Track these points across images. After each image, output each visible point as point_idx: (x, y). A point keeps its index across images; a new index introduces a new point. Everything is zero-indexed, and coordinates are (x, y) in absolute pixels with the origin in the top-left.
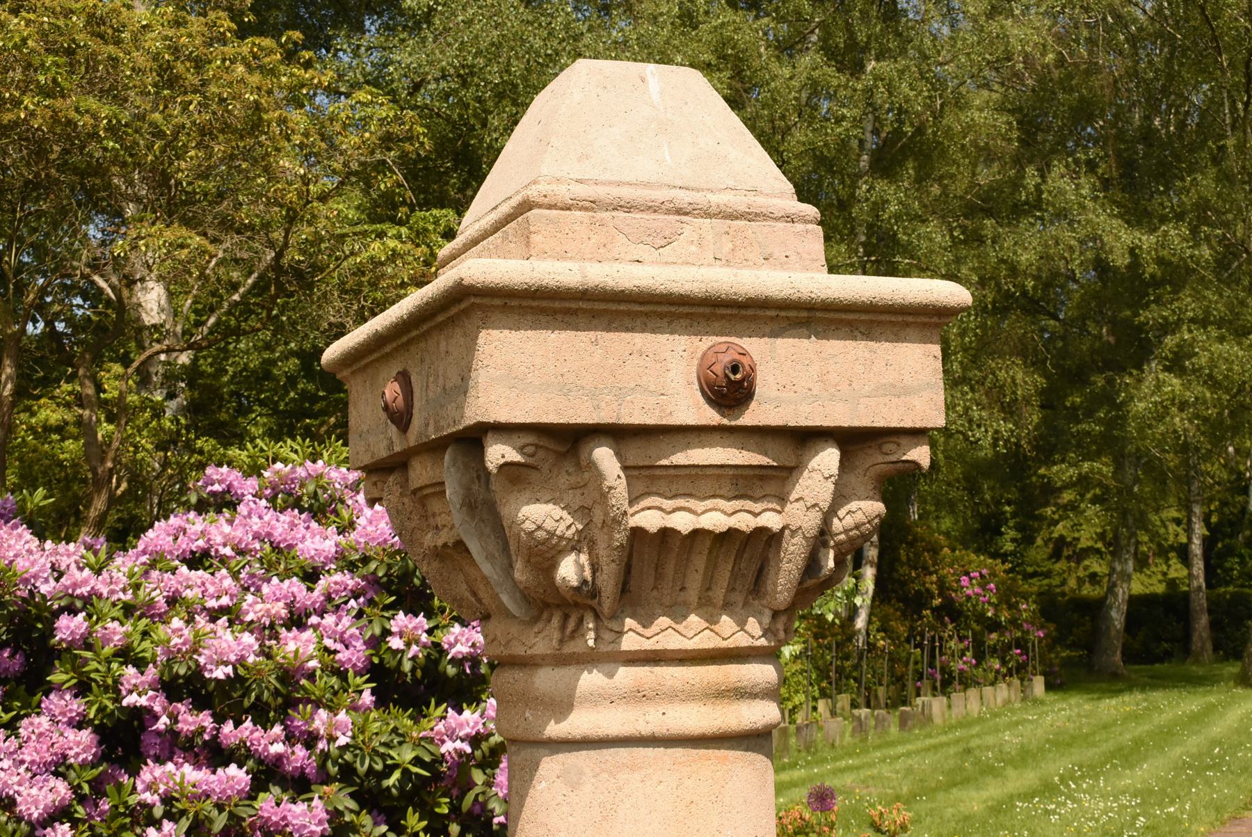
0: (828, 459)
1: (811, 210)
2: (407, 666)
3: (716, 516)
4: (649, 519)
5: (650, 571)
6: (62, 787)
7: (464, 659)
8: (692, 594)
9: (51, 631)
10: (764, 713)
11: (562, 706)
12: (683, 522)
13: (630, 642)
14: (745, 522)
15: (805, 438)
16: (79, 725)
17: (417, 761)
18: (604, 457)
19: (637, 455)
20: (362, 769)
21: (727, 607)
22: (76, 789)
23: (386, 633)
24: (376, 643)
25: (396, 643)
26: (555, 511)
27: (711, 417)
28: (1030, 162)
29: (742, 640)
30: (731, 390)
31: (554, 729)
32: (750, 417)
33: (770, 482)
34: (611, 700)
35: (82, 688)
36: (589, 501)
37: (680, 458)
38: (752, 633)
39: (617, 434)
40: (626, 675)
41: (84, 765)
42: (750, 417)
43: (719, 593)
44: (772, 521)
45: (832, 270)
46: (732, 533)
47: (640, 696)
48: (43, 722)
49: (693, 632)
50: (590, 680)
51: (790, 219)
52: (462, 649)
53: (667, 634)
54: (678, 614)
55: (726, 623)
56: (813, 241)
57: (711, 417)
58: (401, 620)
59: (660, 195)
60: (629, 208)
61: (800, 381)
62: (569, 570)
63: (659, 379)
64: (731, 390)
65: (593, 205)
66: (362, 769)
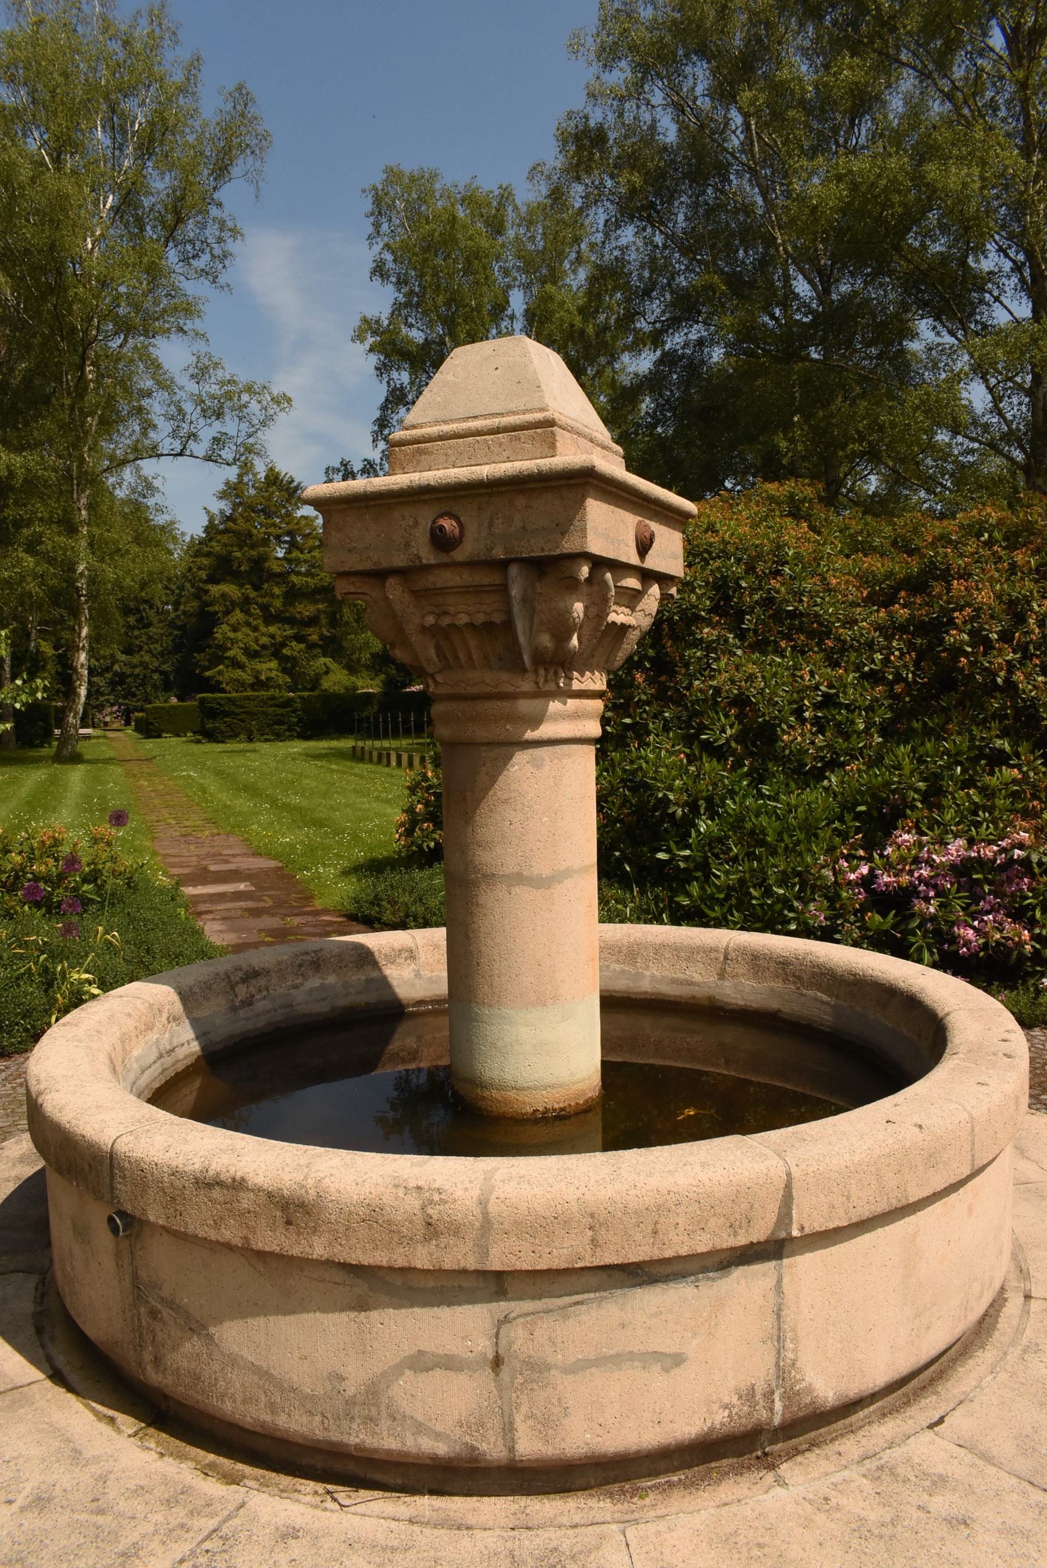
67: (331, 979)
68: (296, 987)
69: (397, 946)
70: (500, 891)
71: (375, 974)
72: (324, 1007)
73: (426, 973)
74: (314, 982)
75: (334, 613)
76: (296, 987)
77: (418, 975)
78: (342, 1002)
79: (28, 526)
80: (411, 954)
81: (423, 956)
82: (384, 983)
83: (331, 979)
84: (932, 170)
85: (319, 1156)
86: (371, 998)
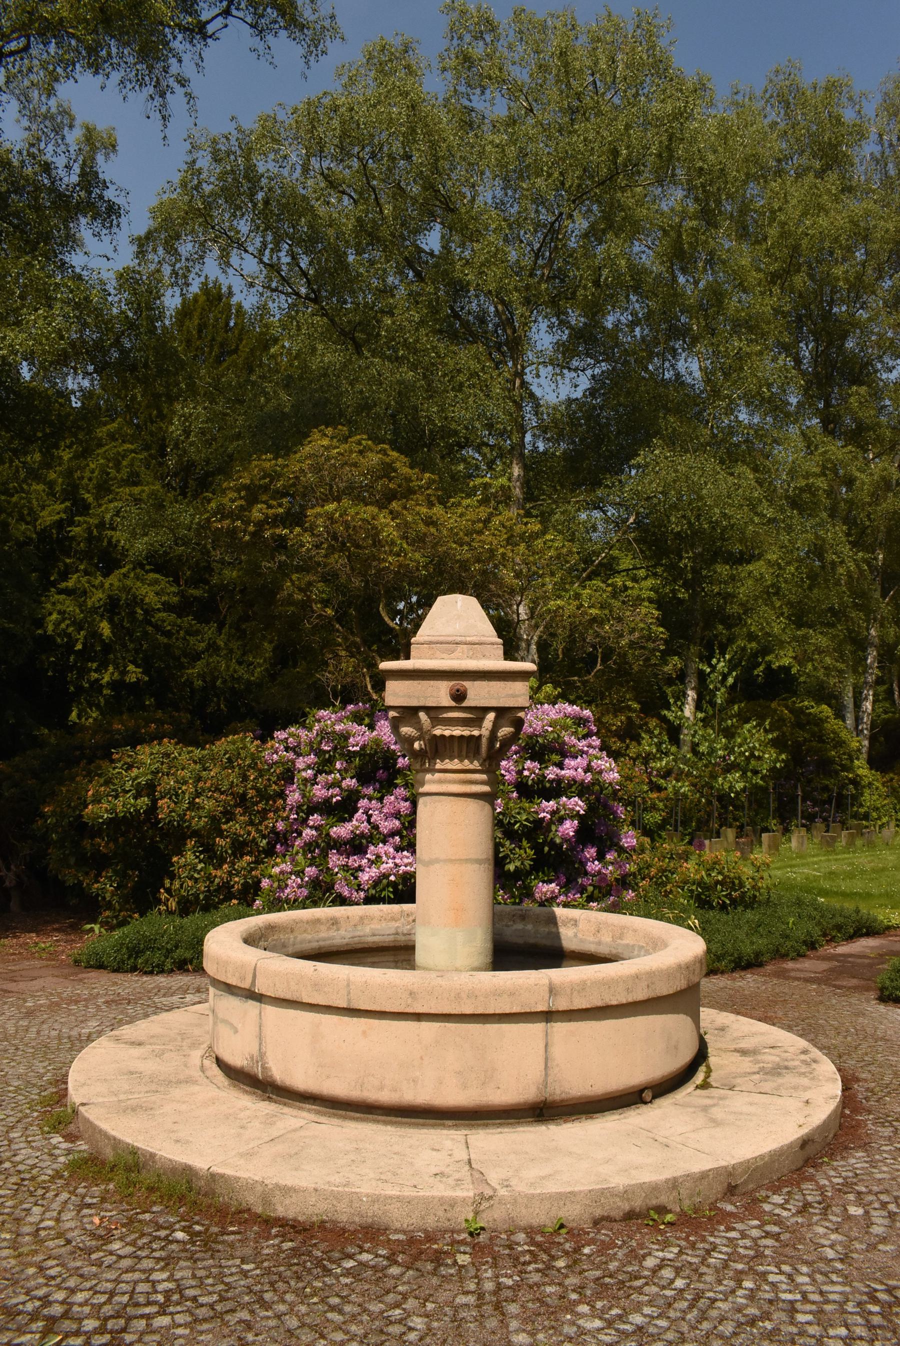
0: (491, 716)
1: (501, 641)
2: (530, 782)
3: (457, 732)
4: (438, 732)
5: (439, 748)
6: (397, 823)
7: (554, 780)
8: (456, 753)
9: (396, 764)
10: (486, 789)
11: (422, 784)
12: (447, 733)
13: (438, 766)
14: (466, 733)
15: (486, 710)
16: (406, 800)
17: (527, 820)
18: (422, 715)
19: (433, 714)
20: (506, 822)
21: (467, 757)
22: (403, 824)
23: (524, 769)
24: (519, 773)
25: (526, 773)
26: (411, 729)
27: (453, 704)
28: (376, 665)
29: (471, 767)
30: (459, 696)
31: (421, 790)
32: (465, 704)
33: (477, 722)
34: (434, 782)
35: (406, 786)
36: (418, 725)
37: (445, 715)
38: (476, 765)
39: (427, 709)
40: (437, 775)
41: (406, 815)
42: (465, 704)
43: (464, 753)
44: (476, 733)
45: (505, 659)
46: (462, 736)
47: (440, 782)
48: (392, 798)
49: (455, 764)
50: (428, 776)
51: (493, 644)
52: (552, 776)
53: (448, 764)
54: (451, 758)
55: (466, 762)
56: (500, 651)
57: (453, 704)
58: (528, 764)
59: (450, 639)
60: (441, 643)
61: (480, 694)
62: (416, 745)
63: (439, 694)
64: (459, 696)
65: (431, 643)
66: (506, 822)
67: (530, 927)
68: (507, 926)
69: (570, 916)
70: (484, 857)
71: (554, 930)
72: (520, 941)
73: (580, 935)
74: (519, 926)
75: (644, 828)
76: (507, 926)
77: (576, 936)
78: (532, 941)
79: (276, 516)
80: (575, 922)
81: (581, 925)
82: (557, 936)
83: (530, 927)
84: (512, 1238)
85: (224, 1163)
86: (547, 942)
